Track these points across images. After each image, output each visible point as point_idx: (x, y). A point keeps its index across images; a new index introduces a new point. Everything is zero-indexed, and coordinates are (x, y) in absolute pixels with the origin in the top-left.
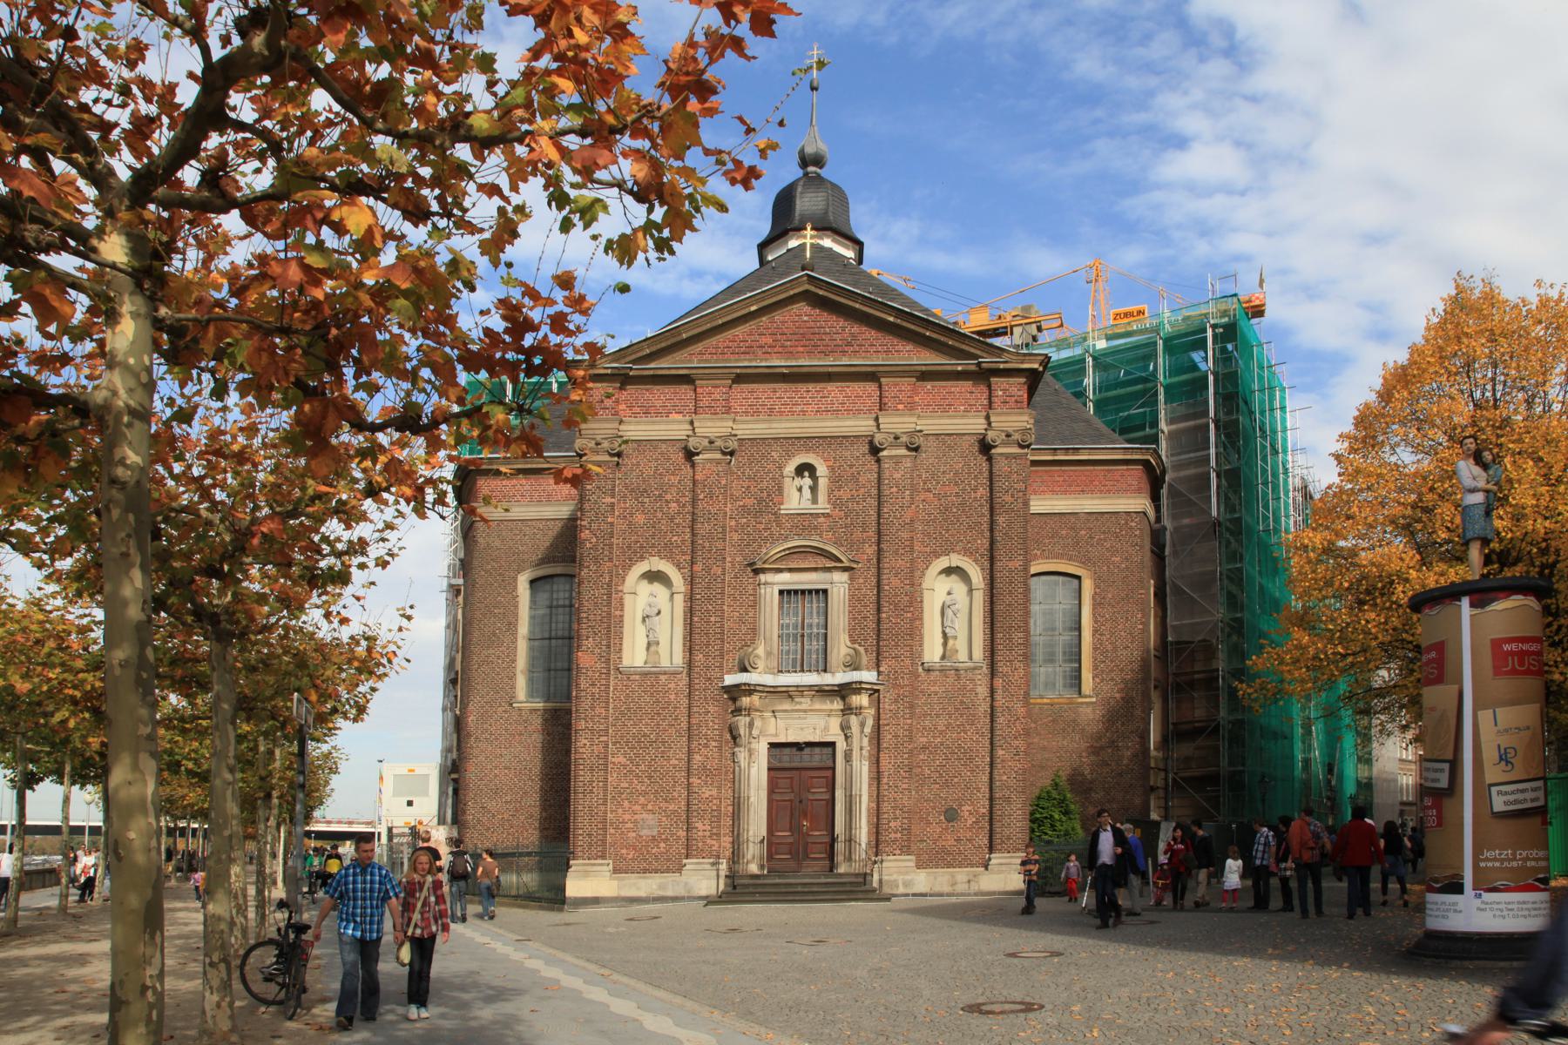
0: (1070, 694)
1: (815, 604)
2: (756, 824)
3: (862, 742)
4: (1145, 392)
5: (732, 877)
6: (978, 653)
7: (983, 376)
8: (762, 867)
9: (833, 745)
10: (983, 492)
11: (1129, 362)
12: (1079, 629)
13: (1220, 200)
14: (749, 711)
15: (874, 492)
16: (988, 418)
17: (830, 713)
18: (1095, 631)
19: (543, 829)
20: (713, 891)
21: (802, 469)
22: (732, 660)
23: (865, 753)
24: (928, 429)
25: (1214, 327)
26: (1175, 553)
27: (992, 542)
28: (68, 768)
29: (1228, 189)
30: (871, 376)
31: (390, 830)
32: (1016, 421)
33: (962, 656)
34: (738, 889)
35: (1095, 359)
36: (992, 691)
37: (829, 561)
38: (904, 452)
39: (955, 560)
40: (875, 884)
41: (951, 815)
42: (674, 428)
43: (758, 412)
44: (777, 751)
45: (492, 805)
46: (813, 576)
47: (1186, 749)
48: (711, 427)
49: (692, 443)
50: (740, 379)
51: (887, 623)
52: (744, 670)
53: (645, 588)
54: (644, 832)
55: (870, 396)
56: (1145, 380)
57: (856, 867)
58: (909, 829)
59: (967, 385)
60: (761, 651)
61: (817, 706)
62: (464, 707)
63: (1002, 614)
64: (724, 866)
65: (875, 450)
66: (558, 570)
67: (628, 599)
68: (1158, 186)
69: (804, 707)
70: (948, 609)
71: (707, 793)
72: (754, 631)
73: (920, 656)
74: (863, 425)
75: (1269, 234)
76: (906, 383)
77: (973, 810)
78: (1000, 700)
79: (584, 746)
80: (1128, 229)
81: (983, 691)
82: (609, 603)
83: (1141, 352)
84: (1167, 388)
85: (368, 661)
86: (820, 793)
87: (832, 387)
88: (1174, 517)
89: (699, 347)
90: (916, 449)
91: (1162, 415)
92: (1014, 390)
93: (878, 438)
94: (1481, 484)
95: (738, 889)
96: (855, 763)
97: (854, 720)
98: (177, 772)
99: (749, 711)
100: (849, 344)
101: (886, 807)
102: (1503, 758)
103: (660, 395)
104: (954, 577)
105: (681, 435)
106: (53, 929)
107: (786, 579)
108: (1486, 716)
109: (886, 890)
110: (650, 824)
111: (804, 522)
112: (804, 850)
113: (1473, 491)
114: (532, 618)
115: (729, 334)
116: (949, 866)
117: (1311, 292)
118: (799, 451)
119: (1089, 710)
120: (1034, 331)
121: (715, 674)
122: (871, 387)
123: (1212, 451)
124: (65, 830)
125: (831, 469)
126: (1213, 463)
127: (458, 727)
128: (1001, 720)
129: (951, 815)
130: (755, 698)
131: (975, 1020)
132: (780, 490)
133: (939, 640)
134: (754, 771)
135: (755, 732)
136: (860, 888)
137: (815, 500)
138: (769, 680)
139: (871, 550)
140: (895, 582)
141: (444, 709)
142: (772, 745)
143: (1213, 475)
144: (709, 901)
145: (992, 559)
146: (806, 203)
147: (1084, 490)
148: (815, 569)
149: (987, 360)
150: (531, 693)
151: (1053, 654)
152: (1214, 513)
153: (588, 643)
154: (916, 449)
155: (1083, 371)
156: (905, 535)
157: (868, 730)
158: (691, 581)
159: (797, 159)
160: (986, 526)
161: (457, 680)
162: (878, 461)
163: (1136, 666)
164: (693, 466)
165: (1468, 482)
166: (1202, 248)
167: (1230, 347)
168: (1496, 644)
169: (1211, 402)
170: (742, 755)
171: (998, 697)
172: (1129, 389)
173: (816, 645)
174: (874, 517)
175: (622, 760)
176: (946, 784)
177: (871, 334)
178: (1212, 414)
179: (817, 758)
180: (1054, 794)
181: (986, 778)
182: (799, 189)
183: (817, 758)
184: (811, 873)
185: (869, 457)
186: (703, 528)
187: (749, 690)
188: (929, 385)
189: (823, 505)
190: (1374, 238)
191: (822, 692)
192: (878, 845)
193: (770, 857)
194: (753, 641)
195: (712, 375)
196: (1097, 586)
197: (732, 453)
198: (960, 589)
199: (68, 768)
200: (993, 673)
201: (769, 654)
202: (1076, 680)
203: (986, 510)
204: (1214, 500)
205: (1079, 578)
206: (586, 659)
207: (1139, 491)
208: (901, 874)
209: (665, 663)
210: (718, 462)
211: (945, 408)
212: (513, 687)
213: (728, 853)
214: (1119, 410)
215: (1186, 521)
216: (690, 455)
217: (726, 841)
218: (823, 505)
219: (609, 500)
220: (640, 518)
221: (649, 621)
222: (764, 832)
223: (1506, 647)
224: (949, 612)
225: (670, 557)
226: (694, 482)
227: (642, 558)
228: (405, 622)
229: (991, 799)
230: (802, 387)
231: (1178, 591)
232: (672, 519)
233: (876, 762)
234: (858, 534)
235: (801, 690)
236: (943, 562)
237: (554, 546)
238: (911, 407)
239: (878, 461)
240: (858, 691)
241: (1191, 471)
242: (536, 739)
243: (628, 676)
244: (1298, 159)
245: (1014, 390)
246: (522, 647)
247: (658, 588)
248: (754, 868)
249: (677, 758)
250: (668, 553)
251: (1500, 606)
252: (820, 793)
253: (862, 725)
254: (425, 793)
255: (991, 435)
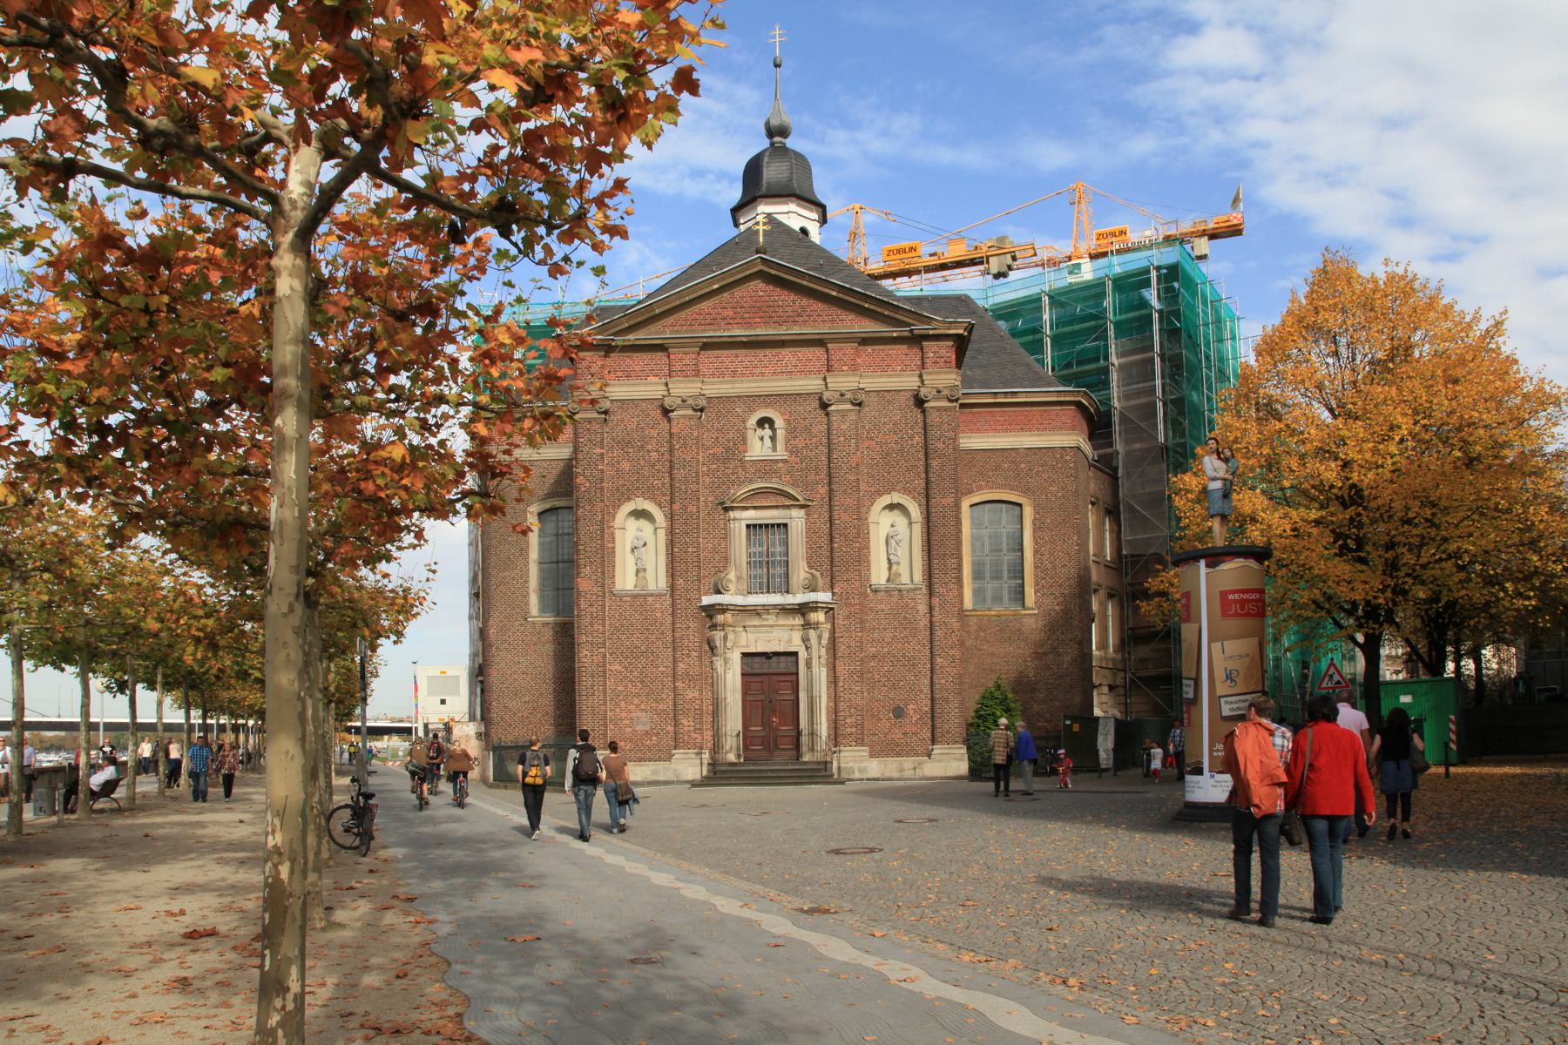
0: (1016, 608)
1: (777, 536)
2: (733, 720)
3: (820, 652)
4: (1096, 328)
5: (713, 764)
6: (918, 577)
7: (916, 340)
8: (739, 756)
9: (795, 654)
10: (918, 439)
11: (1085, 299)
12: (1022, 550)
13: (1235, 86)
14: (723, 626)
15: (825, 440)
16: (921, 376)
17: (792, 628)
18: (1036, 552)
19: (557, 725)
20: (698, 777)
21: (762, 422)
22: (708, 583)
23: (823, 661)
24: (868, 387)
25: (1158, 268)
26: (1128, 475)
27: (927, 483)
28: (159, 678)
29: (1242, 75)
30: (819, 342)
31: (426, 726)
32: (945, 378)
33: (905, 579)
34: (719, 774)
35: (1050, 297)
36: (931, 608)
37: (785, 499)
38: (849, 406)
39: (896, 498)
40: (835, 771)
41: (899, 713)
42: (651, 389)
43: (723, 375)
44: (748, 660)
45: (512, 704)
46: (774, 513)
47: (1143, 651)
48: (683, 388)
49: (668, 402)
50: (707, 346)
51: (839, 552)
52: (718, 592)
53: (633, 524)
54: (639, 728)
55: (818, 359)
56: (1096, 317)
57: (818, 757)
58: (862, 725)
59: (903, 348)
60: (732, 576)
61: (781, 622)
62: (485, 621)
63: (937, 544)
64: (706, 756)
65: (824, 406)
66: (562, 504)
67: (618, 534)
68: (1169, 74)
69: (770, 622)
70: (891, 539)
71: (690, 694)
72: (726, 559)
73: (868, 579)
74: (812, 384)
75: (1286, 120)
76: (849, 348)
77: (917, 708)
78: (938, 616)
79: (586, 657)
80: (1136, 118)
81: (922, 608)
82: (602, 538)
83: (1094, 291)
84: (1117, 325)
85: (405, 605)
86: (786, 694)
87: (786, 352)
88: (1127, 442)
89: (671, 320)
90: (860, 404)
91: (1113, 350)
92: (943, 352)
93: (826, 396)
94: (1221, 474)
95: (719, 774)
96: (815, 669)
97: (812, 634)
98: (244, 680)
99: (723, 626)
100: (799, 315)
101: (842, 706)
102: (1229, 677)
103: (639, 361)
104: (896, 512)
105: (658, 395)
106: (157, 807)
107: (751, 516)
108: (1217, 646)
109: (844, 775)
110: (643, 722)
111: (766, 467)
112: (775, 744)
113: (1214, 479)
114: (541, 544)
115: (696, 308)
116: (898, 755)
117: (1332, 178)
118: (759, 407)
119: (1032, 621)
120: (1010, 261)
121: (693, 595)
122: (819, 351)
123: (1158, 382)
124: (160, 727)
125: (788, 422)
126: (1159, 393)
127: (482, 637)
128: (938, 633)
129: (899, 713)
130: (728, 615)
131: (837, 859)
132: (744, 440)
133: (885, 565)
134: (729, 676)
135: (729, 644)
136: (820, 773)
137: (774, 449)
138: (740, 600)
139: (823, 490)
140: (845, 517)
141: (470, 618)
142: (745, 655)
143: (1160, 405)
144: (694, 784)
145: (928, 497)
146: (772, 172)
147: (1024, 427)
148: (776, 507)
149: (919, 328)
150: (543, 609)
151: (1001, 572)
152: (1161, 439)
153: (586, 571)
154: (860, 404)
155: (1039, 309)
156: (852, 477)
157: (825, 641)
158: (671, 518)
159: (764, 131)
160: (922, 469)
161: (481, 595)
162: (827, 414)
163: (1073, 582)
164: (669, 421)
165: (1210, 473)
166: (1215, 137)
167: (1176, 285)
168: (1223, 594)
169: (1156, 338)
170: (719, 663)
171: (936, 612)
172: (1077, 327)
173: (779, 570)
174: (825, 462)
175: (618, 667)
176: (894, 687)
177: (818, 306)
178: (1157, 348)
179: (783, 665)
180: (997, 694)
181: (927, 682)
182: (766, 159)
183: (783, 665)
184: (779, 763)
185: (819, 412)
186: (680, 473)
187: (723, 609)
188: (869, 349)
189: (781, 453)
190: (1394, 123)
191: (785, 610)
192: (836, 738)
193: (746, 748)
194: (725, 567)
195: (683, 344)
196: (1036, 513)
197: (701, 410)
198: (901, 521)
199: (159, 678)
200: (931, 594)
201: (739, 578)
202: (1019, 594)
203: (921, 455)
204: (1161, 427)
205: (1020, 505)
206: (585, 584)
207: (1073, 428)
208: (857, 762)
209: (652, 587)
210: (690, 417)
211: (883, 368)
212: (527, 604)
213: (710, 745)
214: (1074, 345)
215: (1137, 446)
216: (666, 412)
217: (708, 734)
218: (781, 453)
219: (598, 451)
220: (626, 466)
221: (637, 552)
222: (740, 727)
223: (1231, 597)
224: (892, 542)
225: (653, 498)
226: (671, 434)
227: (629, 499)
228: (431, 575)
229: (932, 699)
230: (760, 353)
231: (1131, 509)
232: (653, 466)
233: (833, 668)
234: (812, 477)
235: (766, 608)
236: (886, 500)
237: (558, 483)
238: (854, 368)
239: (827, 414)
240: (815, 609)
241: (1142, 400)
242: (549, 648)
243: (621, 597)
244: (1312, 42)
245: (943, 352)
246: (534, 570)
247: (643, 523)
248: (732, 757)
249: (664, 666)
250: (650, 494)
251: (1226, 566)
252: (786, 694)
253: (820, 638)
254: (457, 693)
255: (923, 392)
